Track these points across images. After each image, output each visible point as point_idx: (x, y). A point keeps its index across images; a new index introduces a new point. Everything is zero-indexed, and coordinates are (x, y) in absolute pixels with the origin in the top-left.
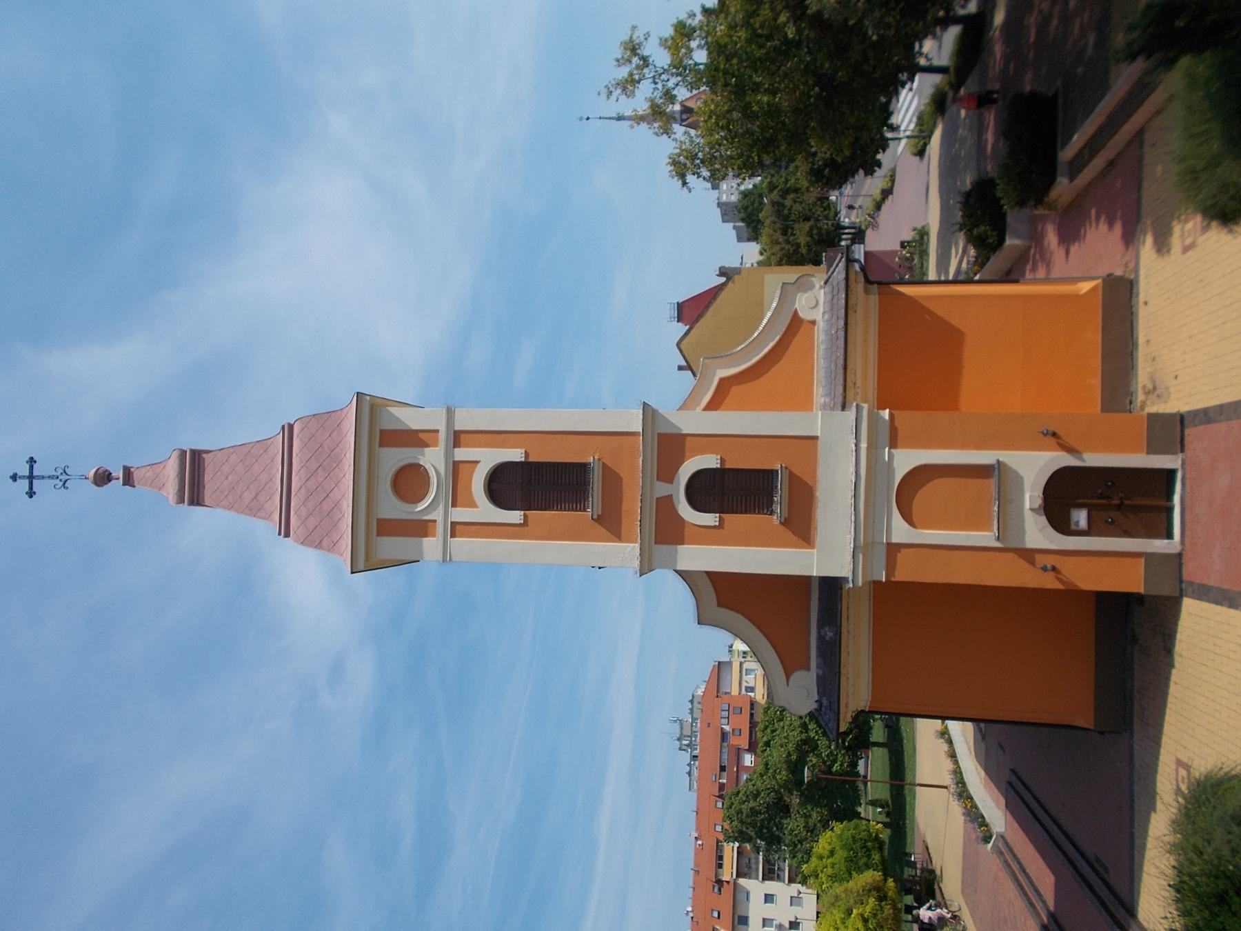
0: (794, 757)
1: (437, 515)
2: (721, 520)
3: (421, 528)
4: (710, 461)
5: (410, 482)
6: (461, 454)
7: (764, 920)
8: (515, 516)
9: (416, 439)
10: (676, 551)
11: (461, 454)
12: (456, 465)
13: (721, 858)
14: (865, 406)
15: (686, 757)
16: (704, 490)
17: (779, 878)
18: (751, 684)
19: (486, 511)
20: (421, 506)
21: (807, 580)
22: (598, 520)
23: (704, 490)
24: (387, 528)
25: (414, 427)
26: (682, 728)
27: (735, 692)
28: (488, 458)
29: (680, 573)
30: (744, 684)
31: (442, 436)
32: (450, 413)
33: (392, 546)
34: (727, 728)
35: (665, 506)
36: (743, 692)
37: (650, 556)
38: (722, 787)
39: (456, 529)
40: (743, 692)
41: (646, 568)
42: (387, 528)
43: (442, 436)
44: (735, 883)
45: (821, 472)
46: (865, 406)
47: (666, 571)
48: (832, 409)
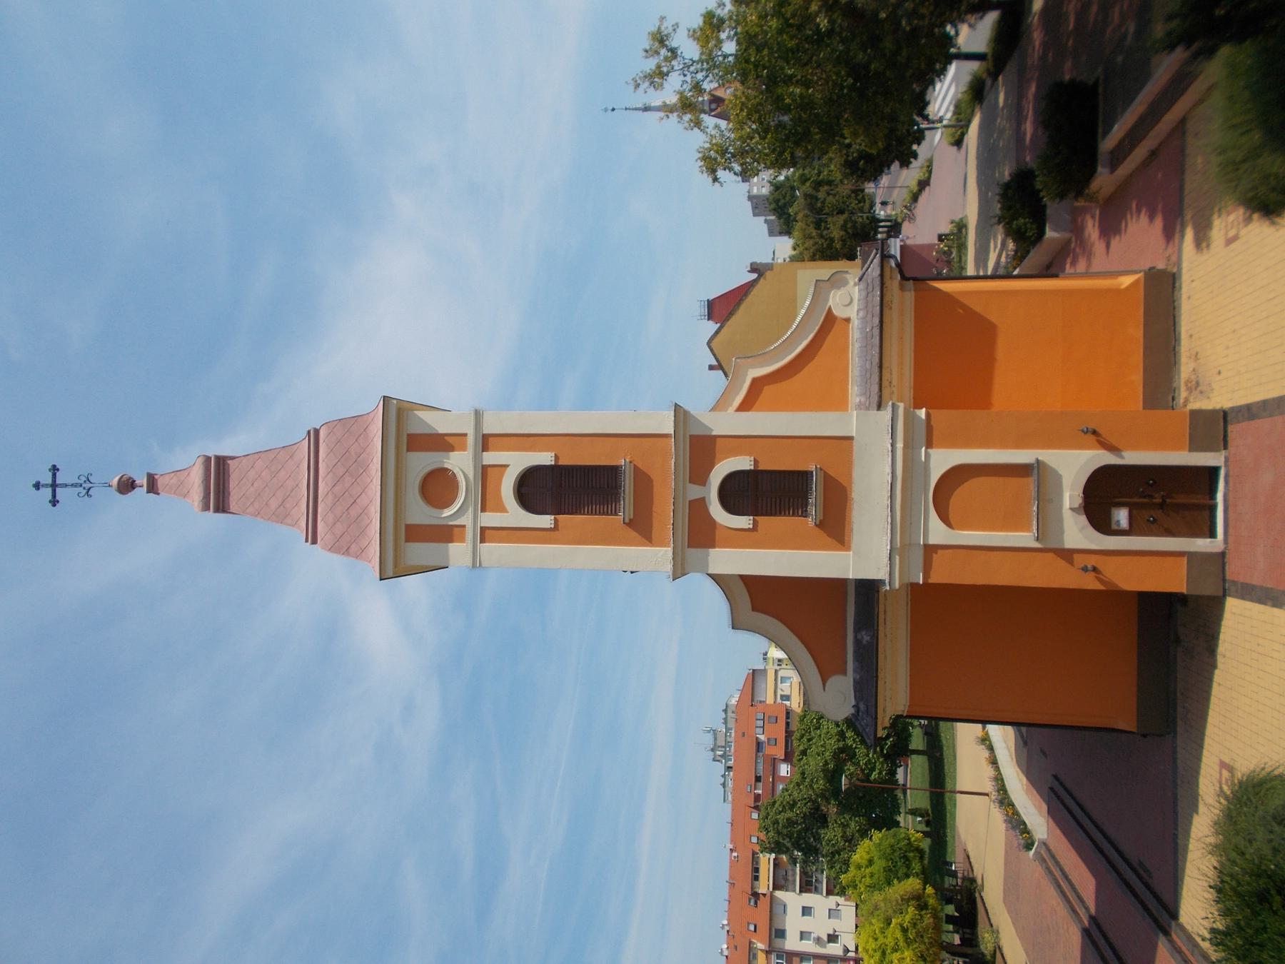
0: (831, 766)
1: (467, 520)
2: (755, 523)
3: (446, 534)
4: (743, 463)
5: (438, 486)
6: (490, 458)
7: (804, 908)
8: (546, 521)
9: (442, 443)
10: (708, 555)
11: (490, 458)
12: (485, 469)
13: (757, 870)
14: (901, 406)
15: (720, 768)
16: (739, 493)
17: (817, 891)
18: (787, 692)
19: (516, 516)
20: (447, 512)
21: (843, 582)
22: (630, 524)
23: (739, 493)
24: (416, 533)
25: (441, 431)
26: (715, 739)
27: (770, 700)
28: (517, 462)
29: (713, 577)
30: (779, 693)
31: (470, 440)
32: (478, 415)
33: (419, 552)
34: (762, 738)
35: (699, 507)
36: (779, 700)
37: (683, 559)
38: (757, 797)
39: (485, 534)
40: (779, 700)
41: (679, 571)
42: (416, 533)
43: (470, 440)
44: (772, 897)
45: (856, 474)
46: (901, 406)
47: (698, 575)
48: (868, 409)
